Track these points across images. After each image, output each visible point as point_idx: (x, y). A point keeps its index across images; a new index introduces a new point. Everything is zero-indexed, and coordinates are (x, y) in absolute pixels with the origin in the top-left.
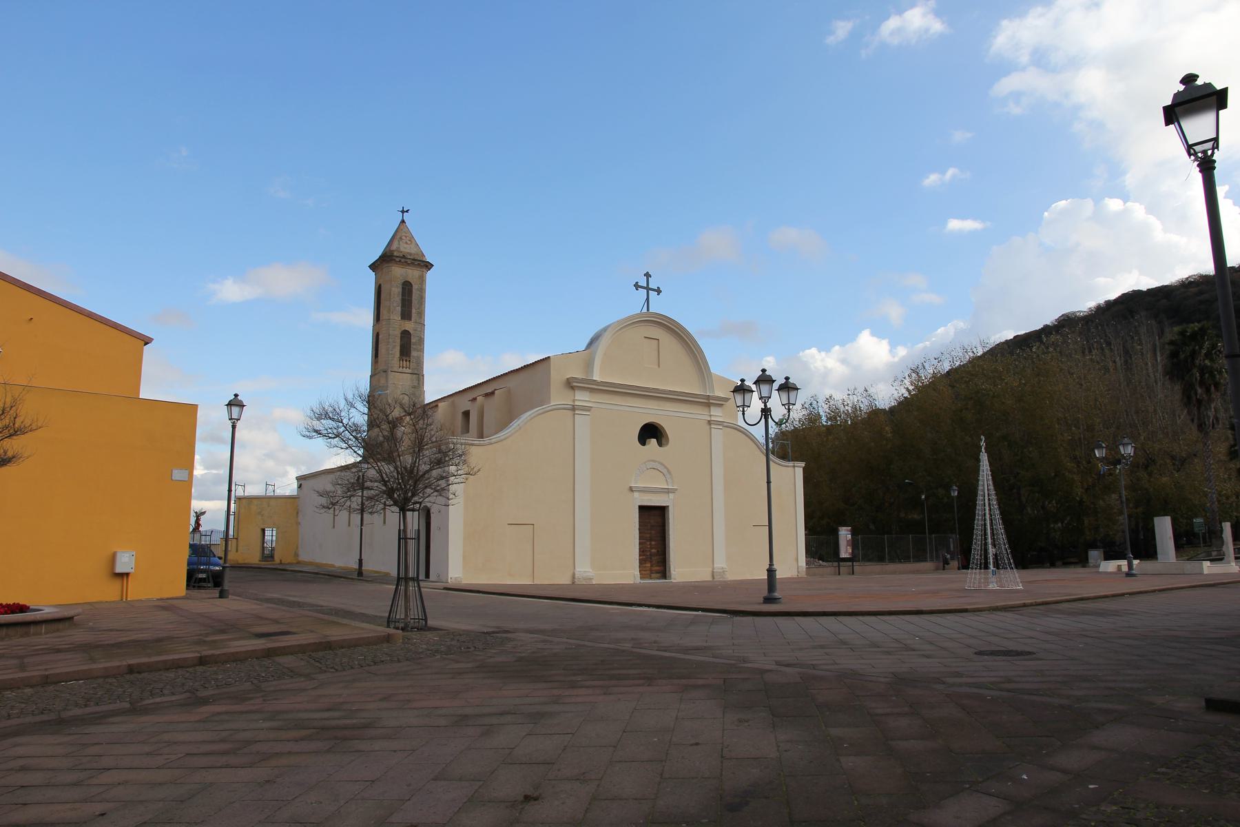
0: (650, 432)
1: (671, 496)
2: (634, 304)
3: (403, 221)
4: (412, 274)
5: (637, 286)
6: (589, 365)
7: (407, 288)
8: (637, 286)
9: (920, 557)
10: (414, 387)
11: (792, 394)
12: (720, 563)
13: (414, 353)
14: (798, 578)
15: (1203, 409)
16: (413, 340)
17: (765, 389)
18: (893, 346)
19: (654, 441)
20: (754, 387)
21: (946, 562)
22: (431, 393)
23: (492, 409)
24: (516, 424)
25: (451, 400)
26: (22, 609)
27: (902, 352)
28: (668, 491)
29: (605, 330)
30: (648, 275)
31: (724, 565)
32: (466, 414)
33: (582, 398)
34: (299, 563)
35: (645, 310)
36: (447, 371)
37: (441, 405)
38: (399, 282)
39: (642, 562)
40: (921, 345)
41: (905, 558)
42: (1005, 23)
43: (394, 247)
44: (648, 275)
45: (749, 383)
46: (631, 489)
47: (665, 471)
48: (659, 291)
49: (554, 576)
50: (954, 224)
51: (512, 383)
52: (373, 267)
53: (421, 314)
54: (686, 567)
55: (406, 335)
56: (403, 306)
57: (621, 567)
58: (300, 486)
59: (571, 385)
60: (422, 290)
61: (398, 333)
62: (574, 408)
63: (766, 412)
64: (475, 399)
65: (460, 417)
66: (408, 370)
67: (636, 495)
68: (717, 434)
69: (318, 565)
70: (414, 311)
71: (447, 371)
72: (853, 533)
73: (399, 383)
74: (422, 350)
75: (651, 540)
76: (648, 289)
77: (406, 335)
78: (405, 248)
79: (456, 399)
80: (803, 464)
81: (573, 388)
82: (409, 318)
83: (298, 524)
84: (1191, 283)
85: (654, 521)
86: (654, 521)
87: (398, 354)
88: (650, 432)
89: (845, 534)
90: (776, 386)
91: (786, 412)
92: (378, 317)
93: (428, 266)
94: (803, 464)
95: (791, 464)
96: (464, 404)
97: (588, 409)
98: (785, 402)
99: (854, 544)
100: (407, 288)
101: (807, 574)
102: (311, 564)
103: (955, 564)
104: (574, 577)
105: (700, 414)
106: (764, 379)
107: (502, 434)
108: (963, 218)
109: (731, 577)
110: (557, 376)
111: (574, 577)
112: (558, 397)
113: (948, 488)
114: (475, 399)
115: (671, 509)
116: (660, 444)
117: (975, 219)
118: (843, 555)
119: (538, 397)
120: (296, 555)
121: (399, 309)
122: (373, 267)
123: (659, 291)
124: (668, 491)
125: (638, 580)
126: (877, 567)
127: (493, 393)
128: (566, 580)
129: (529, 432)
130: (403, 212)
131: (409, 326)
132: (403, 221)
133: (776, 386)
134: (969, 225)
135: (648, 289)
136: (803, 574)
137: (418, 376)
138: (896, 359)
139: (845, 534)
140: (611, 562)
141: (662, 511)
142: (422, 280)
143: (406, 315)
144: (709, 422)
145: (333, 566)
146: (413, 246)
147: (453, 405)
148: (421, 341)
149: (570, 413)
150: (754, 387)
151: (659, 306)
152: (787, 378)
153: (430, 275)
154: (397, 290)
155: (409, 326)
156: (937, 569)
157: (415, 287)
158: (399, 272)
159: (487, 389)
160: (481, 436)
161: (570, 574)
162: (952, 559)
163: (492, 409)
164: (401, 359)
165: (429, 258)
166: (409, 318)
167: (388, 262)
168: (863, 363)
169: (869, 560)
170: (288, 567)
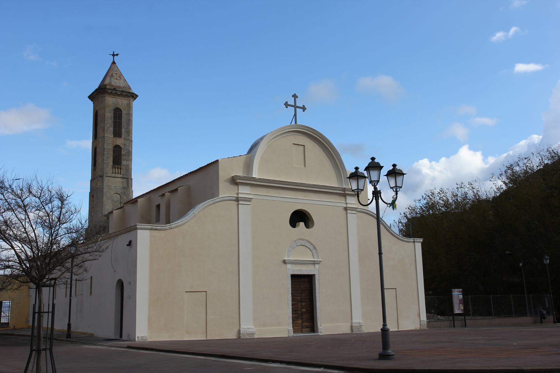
0: (300, 217)
2: (285, 118)
3: (114, 63)
4: (121, 102)
5: (287, 105)
6: (249, 165)
7: (118, 113)
8: (287, 105)
9: (521, 313)
10: (124, 188)
11: (399, 179)
12: (357, 319)
13: (124, 163)
14: (421, 330)
16: (123, 153)
17: (374, 175)
18: (485, 156)
20: (366, 173)
21: (543, 317)
22: (137, 191)
23: (176, 201)
24: (191, 214)
25: (148, 196)
27: (492, 160)
28: (314, 263)
29: (262, 139)
30: (295, 96)
31: (361, 321)
32: (158, 206)
33: (244, 191)
35: (293, 123)
36: (148, 174)
37: (139, 200)
39: (294, 319)
40: (505, 155)
41: (509, 313)
43: (107, 82)
44: (295, 96)
45: (362, 170)
46: (284, 262)
48: (304, 108)
49: (222, 332)
50: (520, 68)
51: (191, 182)
52: (91, 97)
53: (129, 133)
54: (329, 323)
55: (117, 150)
56: (115, 126)
59: (234, 181)
60: (129, 115)
61: (111, 147)
62: (237, 200)
63: (377, 194)
64: (164, 195)
65: (154, 209)
66: (119, 176)
67: (289, 266)
68: (353, 218)
70: (123, 130)
71: (148, 174)
72: (464, 294)
73: (113, 183)
74: (130, 160)
75: (301, 302)
76: (295, 107)
77: (117, 150)
78: (115, 83)
80: (421, 240)
81: (237, 184)
85: (303, 289)
86: (303, 289)
87: (111, 164)
88: (300, 217)
89: (457, 294)
90: (384, 171)
91: (394, 194)
93: (134, 96)
94: (421, 240)
95: (412, 240)
96: (157, 200)
97: (249, 200)
98: (393, 185)
99: (465, 302)
100: (118, 113)
103: (550, 318)
104: (239, 332)
105: (339, 202)
106: (374, 166)
107: (180, 222)
108: (527, 62)
110: (224, 174)
111: (239, 332)
112: (226, 191)
114: (164, 195)
115: (317, 277)
116: (307, 226)
117: (536, 63)
118: (457, 311)
119: (211, 192)
121: (112, 129)
122: (91, 97)
123: (304, 108)
124: (314, 263)
125: (292, 334)
126: (485, 321)
127: (176, 190)
128: (232, 335)
129: (202, 219)
130: (114, 55)
131: (119, 142)
132: (114, 63)
133: (384, 171)
134: (532, 67)
135: (295, 107)
136: (425, 327)
137: (128, 180)
138: (488, 166)
139: (457, 294)
141: (310, 279)
142: (129, 107)
143: (117, 133)
146: (122, 81)
147: (149, 201)
148: (129, 153)
150: (366, 173)
151: (304, 120)
152: (394, 166)
153: (135, 104)
154: (109, 115)
155: (119, 142)
156: (535, 322)
157: (124, 112)
158: (110, 101)
159: (171, 187)
160: (168, 222)
162: (548, 313)
163: (176, 201)
164: (114, 167)
165: (134, 90)
168: (464, 165)
169: (481, 315)
170: (17, 333)
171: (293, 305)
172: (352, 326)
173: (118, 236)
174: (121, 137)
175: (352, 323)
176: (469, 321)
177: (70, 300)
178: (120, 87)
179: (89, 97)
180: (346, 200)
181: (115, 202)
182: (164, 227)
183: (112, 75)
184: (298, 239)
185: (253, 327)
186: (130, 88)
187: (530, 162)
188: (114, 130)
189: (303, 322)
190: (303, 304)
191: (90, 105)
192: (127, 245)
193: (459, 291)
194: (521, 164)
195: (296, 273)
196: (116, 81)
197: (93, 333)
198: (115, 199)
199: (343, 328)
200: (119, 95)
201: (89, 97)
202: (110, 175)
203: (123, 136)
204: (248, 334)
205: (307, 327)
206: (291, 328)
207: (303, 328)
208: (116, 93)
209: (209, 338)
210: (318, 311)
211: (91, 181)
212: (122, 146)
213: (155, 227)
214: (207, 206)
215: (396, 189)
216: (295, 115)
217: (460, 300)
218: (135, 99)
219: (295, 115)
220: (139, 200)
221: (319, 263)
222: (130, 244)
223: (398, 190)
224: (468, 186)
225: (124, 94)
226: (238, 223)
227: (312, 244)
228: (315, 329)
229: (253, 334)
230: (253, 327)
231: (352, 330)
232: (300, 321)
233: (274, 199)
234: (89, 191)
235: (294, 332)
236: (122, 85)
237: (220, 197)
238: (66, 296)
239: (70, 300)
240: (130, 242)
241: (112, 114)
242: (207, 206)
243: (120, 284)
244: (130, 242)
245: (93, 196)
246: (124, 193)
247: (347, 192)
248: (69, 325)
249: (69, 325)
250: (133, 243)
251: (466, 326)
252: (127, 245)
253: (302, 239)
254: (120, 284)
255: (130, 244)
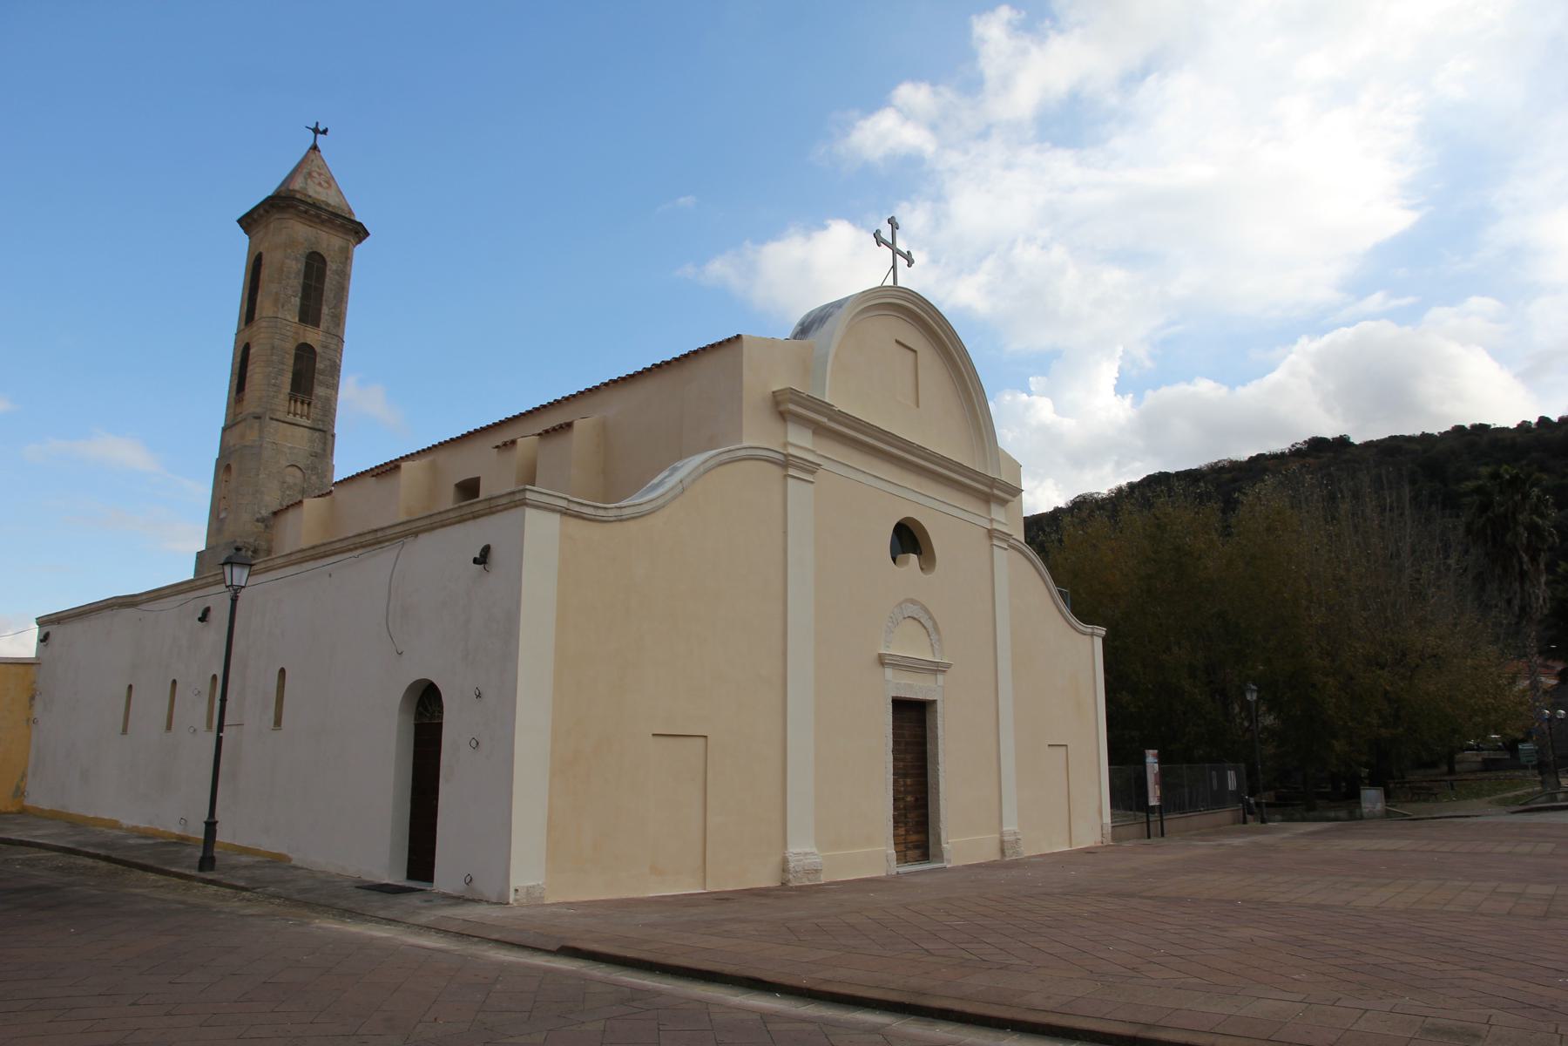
3: (315, 148)
4: (329, 241)
7: (315, 266)
10: (316, 455)
13: (319, 391)
15: (1527, 586)
16: (320, 365)
19: (913, 557)
22: (346, 463)
26: (214, 677)
28: (937, 669)
30: (892, 222)
34: (23, 811)
35: (889, 282)
37: (404, 465)
38: (300, 256)
43: (297, 185)
46: (882, 661)
47: (929, 624)
51: (615, 407)
52: (248, 222)
53: (338, 319)
54: (963, 838)
55: (305, 354)
58: (44, 639)
61: (291, 347)
66: (304, 421)
67: (889, 672)
69: (75, 823)
70: (325, 310)
74: (335, 387)
77: (305, 354)
78: (316, 192)
79: (441, 457)
81: (783, 416)
82: (316, 323)
83: (31, 721)
84: (1223, 468)
92: (249, 315)
94: (1102, 631)
96: (462, 467)
97: (811, 468)
100: (315, 266)
101: (1114, 838)
102: (54, 816)
104: (784, 867)
111: (784, 867)
115: (940, 706)
120: (19, 792)
121: (296, 301)
122: (248, 222)
124: (937, 669)
125: (895, 868)
129: (696, 501)
130: (316, 131)
132: (315, 148)
137: (324, 434)
140: (836, 832)
142: (346, 258)
143: (309, 314)
144: (991, 534)
145: (115, 825)
146: (332, 192)
148: (334, 369)
149: (776, 471)
153: (360, 252)
155: (313, 337)
157: (332, 266)
161: (775, 860)
164: (293, 397)
166: (316, 323)
167: (282, 209)
172: (1002, 842)
173: (416, 534)
174: (318, 326)
175: (1002, 834)
176: (1174, 822)
177: (219, 741)
179: (239, 221)
180: (989, 512)
181: (289, 488)
182: (601, 513)
183: (310, 174)
184: (907, 600)
185: (814, 850)
186: (351, 212)
188: (302, 305)
190: (909, 781)
191: (241, 242)
192: (475, 561)
196: (319, 189)
197: (284, 851)
198: (290, 480)
200: (323, 222)
201: (239, 221)
202: (279, 415)
203: (323, 325)
204: (807, 872)
208: (318, 216)
209: (709, 889)
210: (942, 803)
211: (224, 430)
212: (318, 349)
213: (577, 508)
214: (713, 468)
216: (894, 267)
218: (360, 241)
219: (894, 267)
220: (404, 465)
222: (483, 558)
225: (339, 221)
226: (785, 532)
227: (931, 618)
228: (932, 850)
229: (817, 871)
230: (814, 850)
231: (1003, 852)
233: (861, 477)
234: (215, 454)
236: (331, 202)
237: (745, 444)
239: (219, 741)
240: (207, 611)
241: (301, 266)
242: (713, 468)
243: (426, 703)
244: (486, 550)
245: (228, 467)
246: (314, 468)
247: (996, 492)
248: (211, 826)
249: (211, 826)
250: (495, 555)
252: (475, 561)
253: (913, 602)
254: (426, 703)
255: (483, 558)
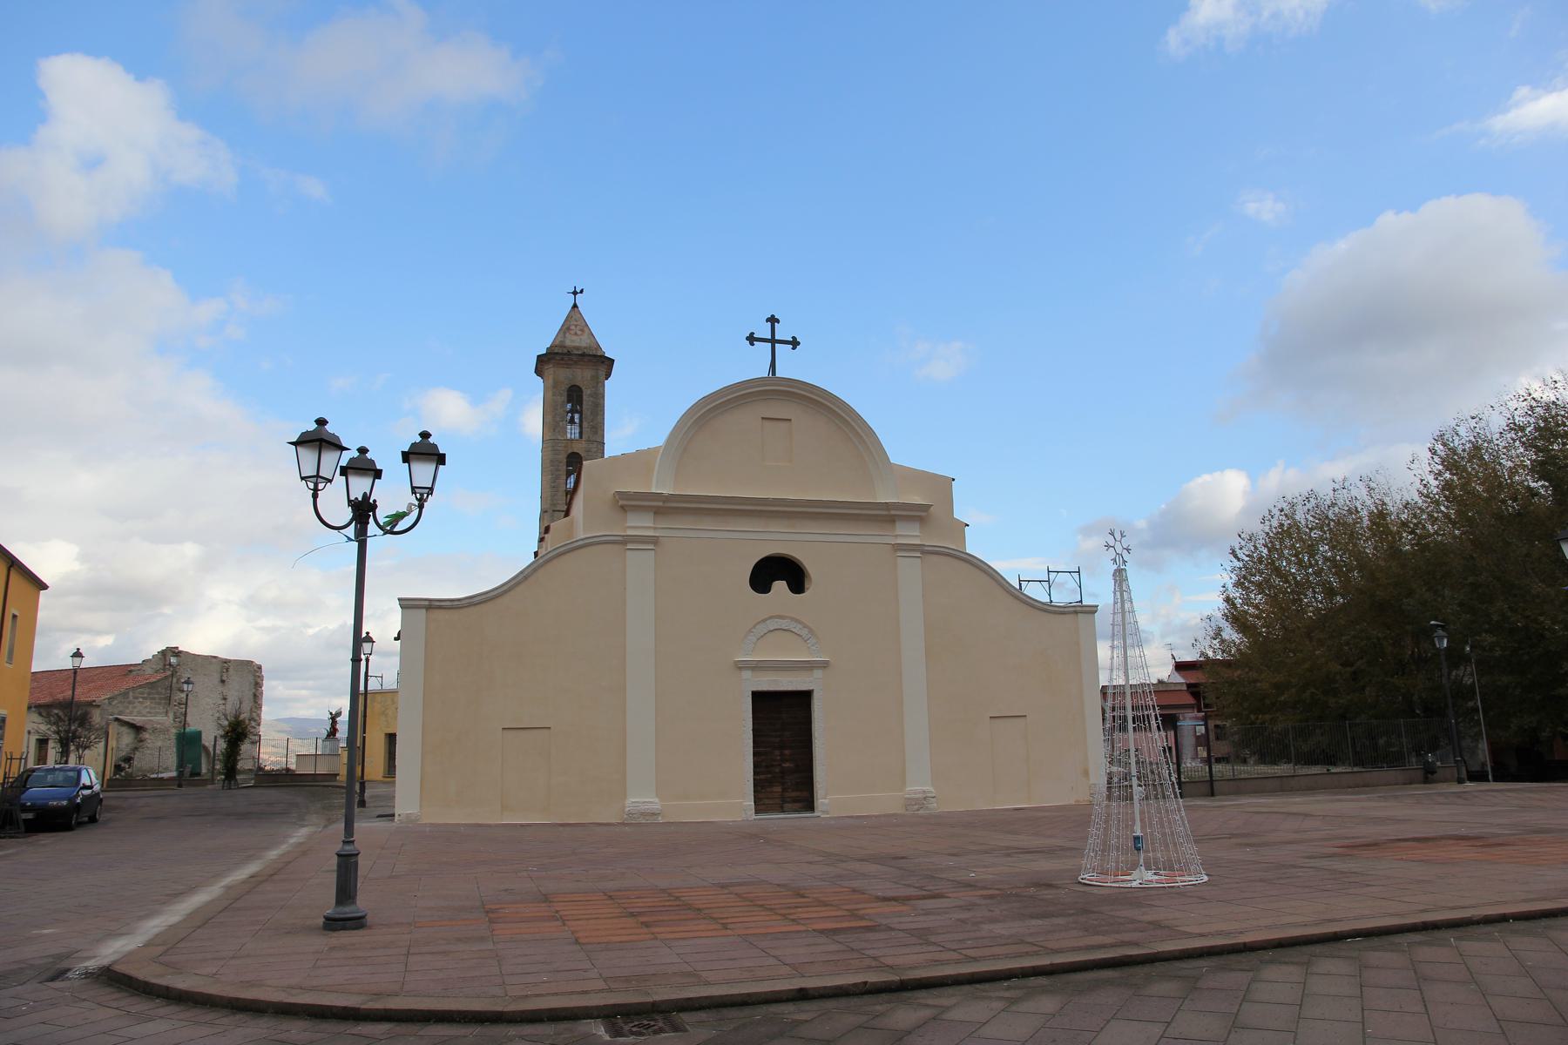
1: (818, 673)
3: (575, 306)
12: (919, 783)
28: (809, 666)
30: (773, 320)
33: (640, 524)
42: (1523, 91)
44: (773, 320)
57: (726, 787)
67: (747, 674)
71: (14, 576)
76: (773, 341)
85: (783, 724)
86: (783, 724)
88: (778, 571)
109: (935, 807)
113: (1428, 633)
130: (575, 293)
132: (575, 306)
135: (773, 341)
141: (801, 700)
146: (585, 337)
151: (791, 366)
157: (587, 392)
171: (755, 754)
178: (577, 348)
187: (1483, 424)
189: (784, 790)
190: (787, 752)
193: (1197, 718)
194: (1462, 431)
195: (760, 688)
199: (882, 801)
205: (795, 801)
206: (750, 802)
207: (784, 801)
215: (316, 485)
217: (1197, 738)
221: (824, 665)
223: (321, 486)
224: (1360, 484)
232: (779, 789)
235: (757, 812)
236: (583, 344)
238: (391, 738)
251: (1213, 795)
